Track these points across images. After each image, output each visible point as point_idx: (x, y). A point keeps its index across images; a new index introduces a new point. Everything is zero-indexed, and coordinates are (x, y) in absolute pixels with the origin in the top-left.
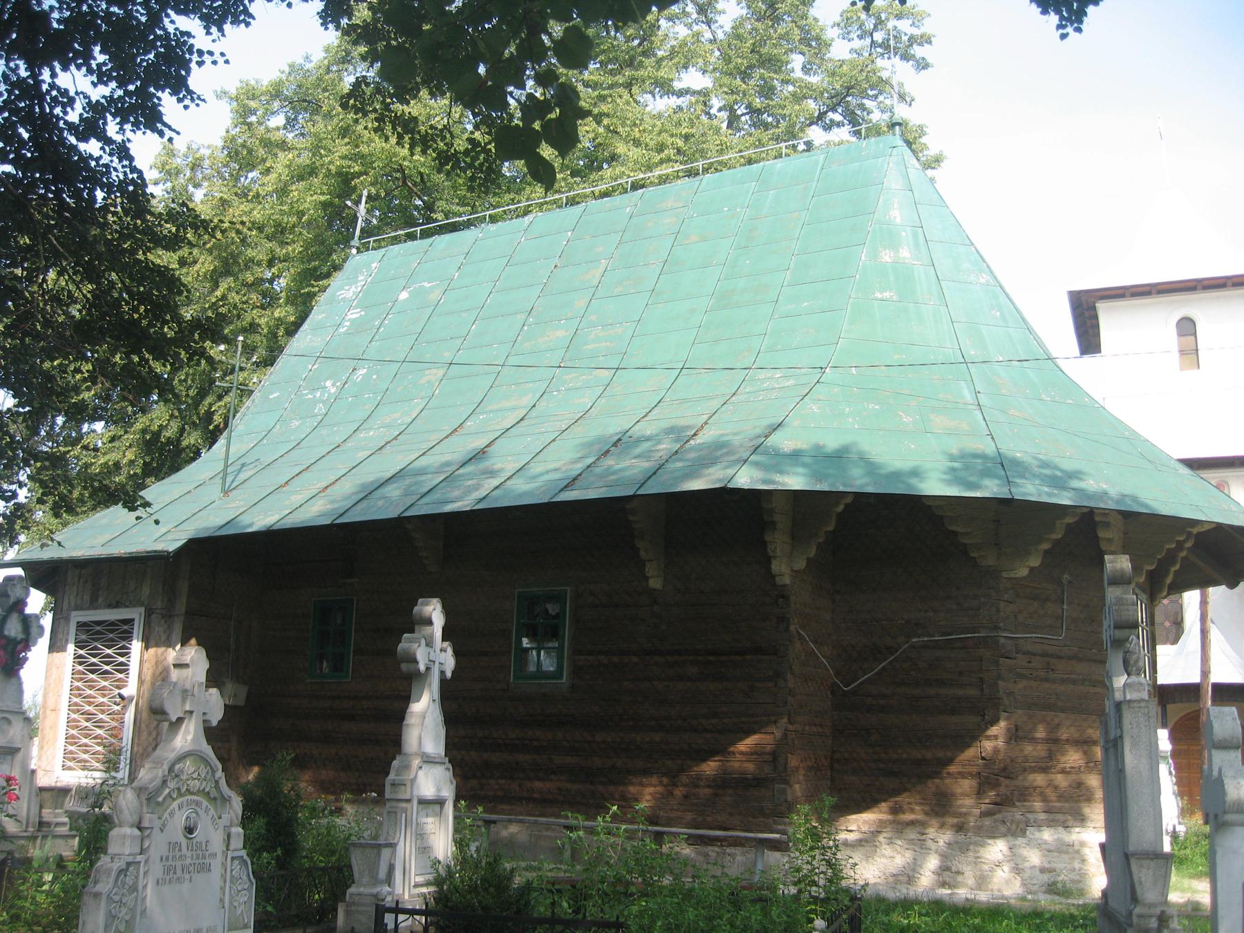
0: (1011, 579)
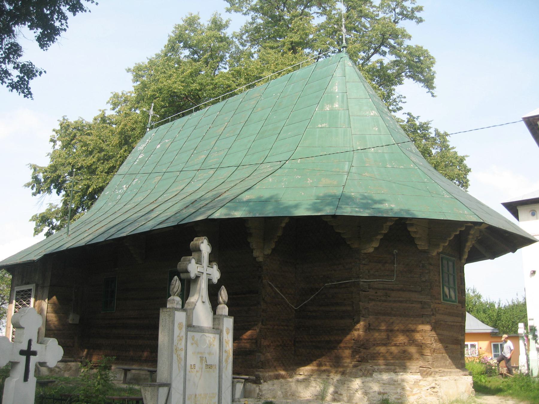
0: (365, 253)
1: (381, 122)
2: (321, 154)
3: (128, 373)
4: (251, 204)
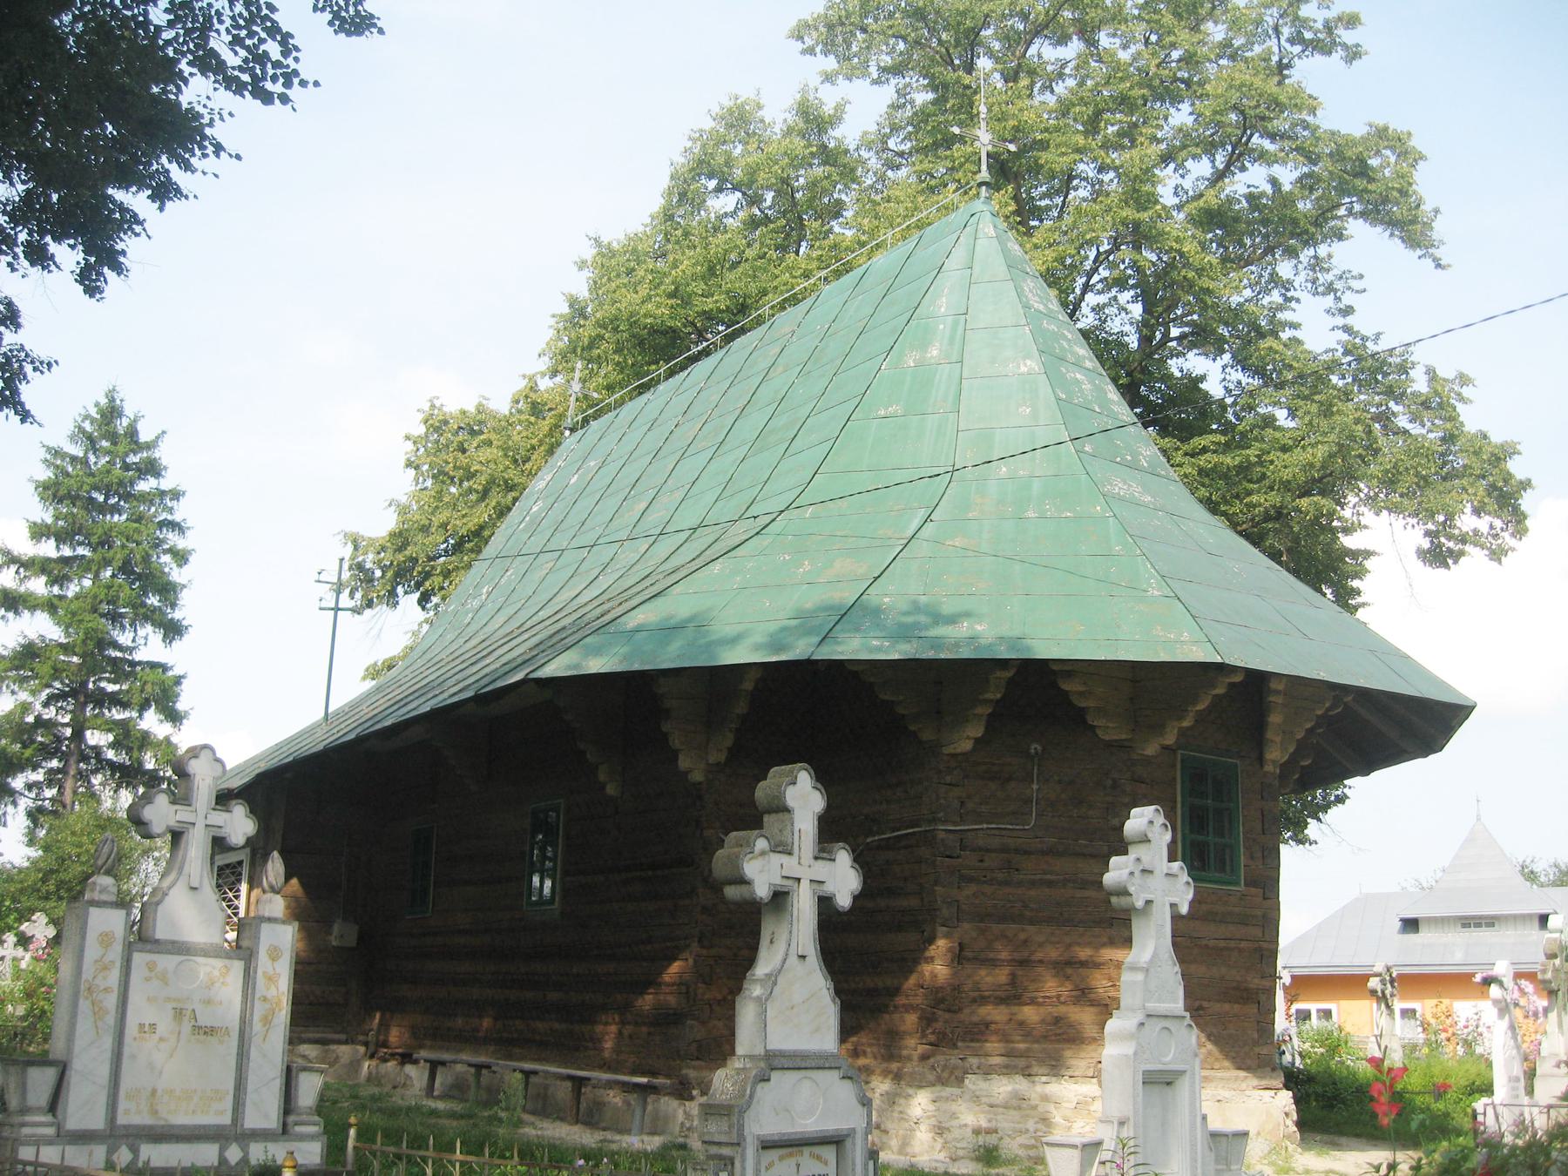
0: (954, 755)
1: (1045, 390)
4: (639, 636)
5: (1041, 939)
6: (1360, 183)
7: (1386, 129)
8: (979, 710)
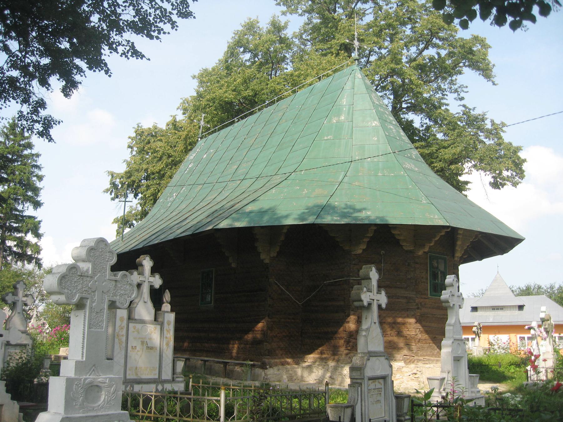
0: (356, 255)
2: (324, 165)
3: (207, 363)
4: (252, 214)
5: (384, 315)
6: (470, 56)
7: (478, 37)
8: (364, 240)
